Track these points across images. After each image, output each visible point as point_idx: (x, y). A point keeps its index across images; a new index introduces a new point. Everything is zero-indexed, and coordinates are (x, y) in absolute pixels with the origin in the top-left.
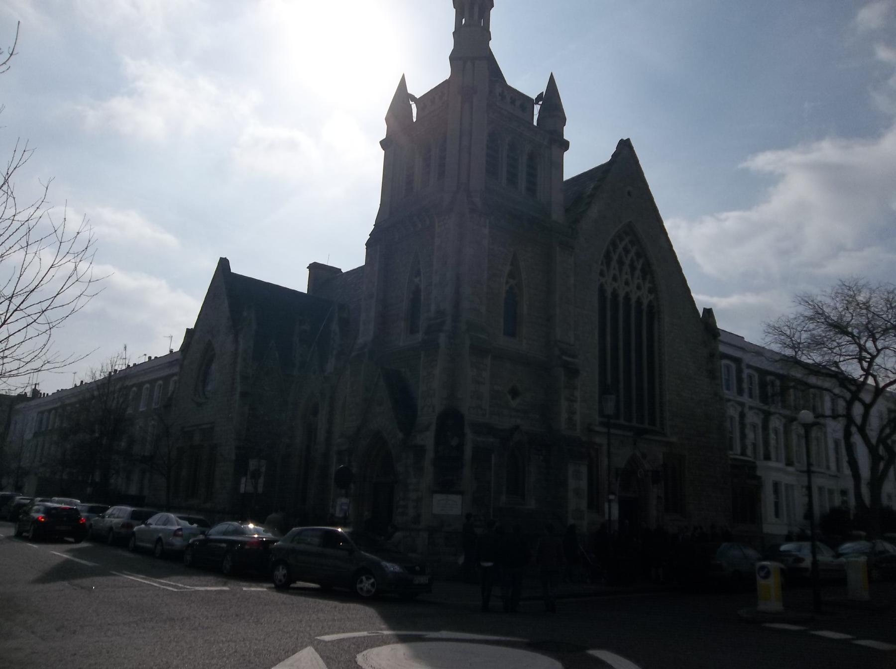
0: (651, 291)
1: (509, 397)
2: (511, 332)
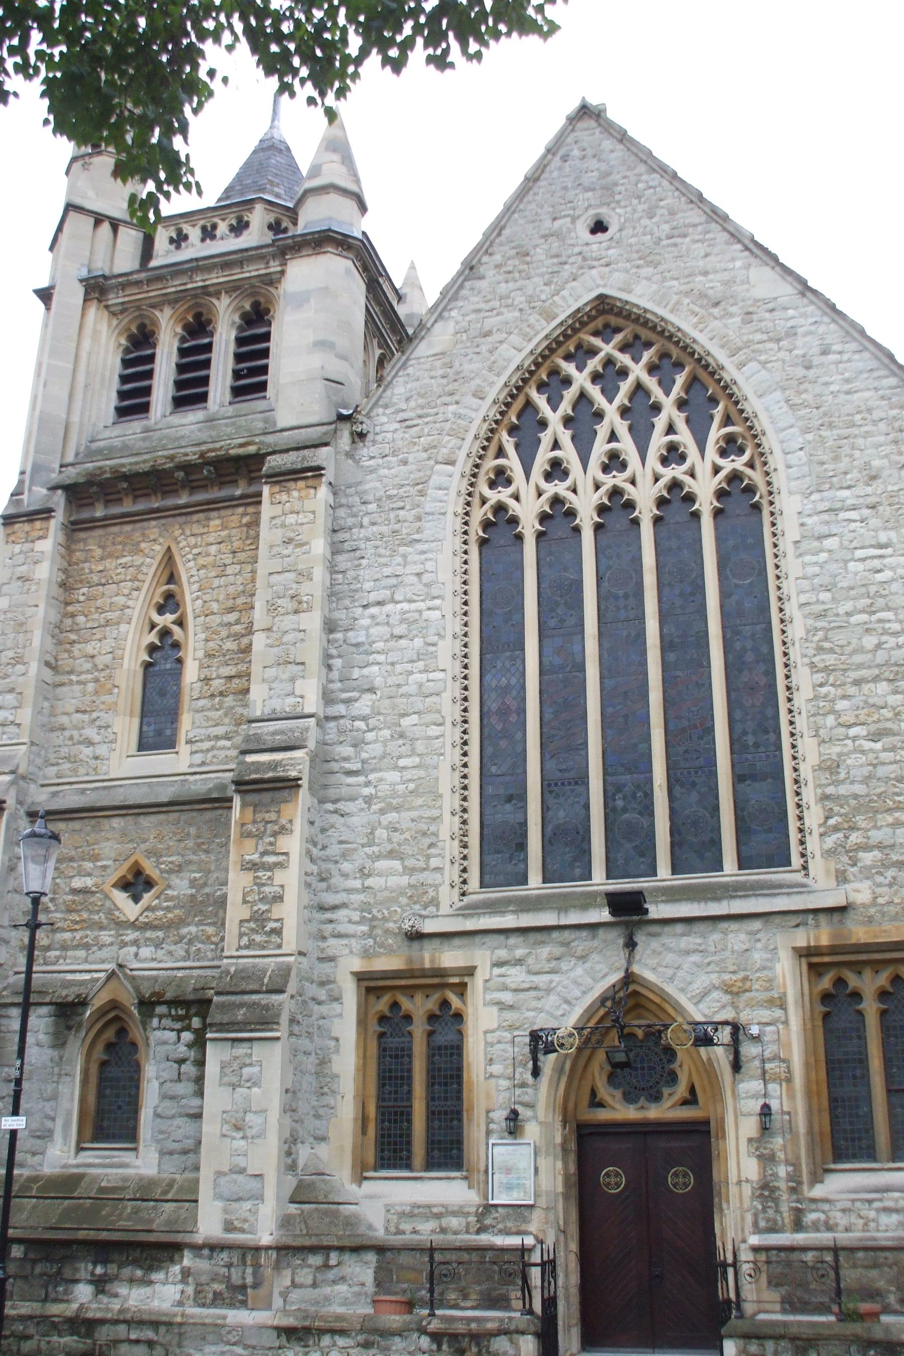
0: (730, 446)
1: (121, 898)
2: (158, 728)
